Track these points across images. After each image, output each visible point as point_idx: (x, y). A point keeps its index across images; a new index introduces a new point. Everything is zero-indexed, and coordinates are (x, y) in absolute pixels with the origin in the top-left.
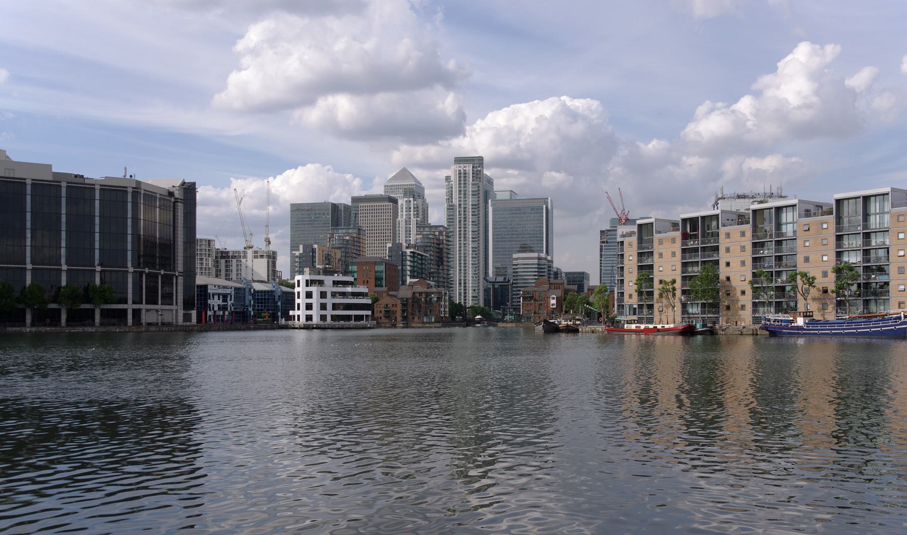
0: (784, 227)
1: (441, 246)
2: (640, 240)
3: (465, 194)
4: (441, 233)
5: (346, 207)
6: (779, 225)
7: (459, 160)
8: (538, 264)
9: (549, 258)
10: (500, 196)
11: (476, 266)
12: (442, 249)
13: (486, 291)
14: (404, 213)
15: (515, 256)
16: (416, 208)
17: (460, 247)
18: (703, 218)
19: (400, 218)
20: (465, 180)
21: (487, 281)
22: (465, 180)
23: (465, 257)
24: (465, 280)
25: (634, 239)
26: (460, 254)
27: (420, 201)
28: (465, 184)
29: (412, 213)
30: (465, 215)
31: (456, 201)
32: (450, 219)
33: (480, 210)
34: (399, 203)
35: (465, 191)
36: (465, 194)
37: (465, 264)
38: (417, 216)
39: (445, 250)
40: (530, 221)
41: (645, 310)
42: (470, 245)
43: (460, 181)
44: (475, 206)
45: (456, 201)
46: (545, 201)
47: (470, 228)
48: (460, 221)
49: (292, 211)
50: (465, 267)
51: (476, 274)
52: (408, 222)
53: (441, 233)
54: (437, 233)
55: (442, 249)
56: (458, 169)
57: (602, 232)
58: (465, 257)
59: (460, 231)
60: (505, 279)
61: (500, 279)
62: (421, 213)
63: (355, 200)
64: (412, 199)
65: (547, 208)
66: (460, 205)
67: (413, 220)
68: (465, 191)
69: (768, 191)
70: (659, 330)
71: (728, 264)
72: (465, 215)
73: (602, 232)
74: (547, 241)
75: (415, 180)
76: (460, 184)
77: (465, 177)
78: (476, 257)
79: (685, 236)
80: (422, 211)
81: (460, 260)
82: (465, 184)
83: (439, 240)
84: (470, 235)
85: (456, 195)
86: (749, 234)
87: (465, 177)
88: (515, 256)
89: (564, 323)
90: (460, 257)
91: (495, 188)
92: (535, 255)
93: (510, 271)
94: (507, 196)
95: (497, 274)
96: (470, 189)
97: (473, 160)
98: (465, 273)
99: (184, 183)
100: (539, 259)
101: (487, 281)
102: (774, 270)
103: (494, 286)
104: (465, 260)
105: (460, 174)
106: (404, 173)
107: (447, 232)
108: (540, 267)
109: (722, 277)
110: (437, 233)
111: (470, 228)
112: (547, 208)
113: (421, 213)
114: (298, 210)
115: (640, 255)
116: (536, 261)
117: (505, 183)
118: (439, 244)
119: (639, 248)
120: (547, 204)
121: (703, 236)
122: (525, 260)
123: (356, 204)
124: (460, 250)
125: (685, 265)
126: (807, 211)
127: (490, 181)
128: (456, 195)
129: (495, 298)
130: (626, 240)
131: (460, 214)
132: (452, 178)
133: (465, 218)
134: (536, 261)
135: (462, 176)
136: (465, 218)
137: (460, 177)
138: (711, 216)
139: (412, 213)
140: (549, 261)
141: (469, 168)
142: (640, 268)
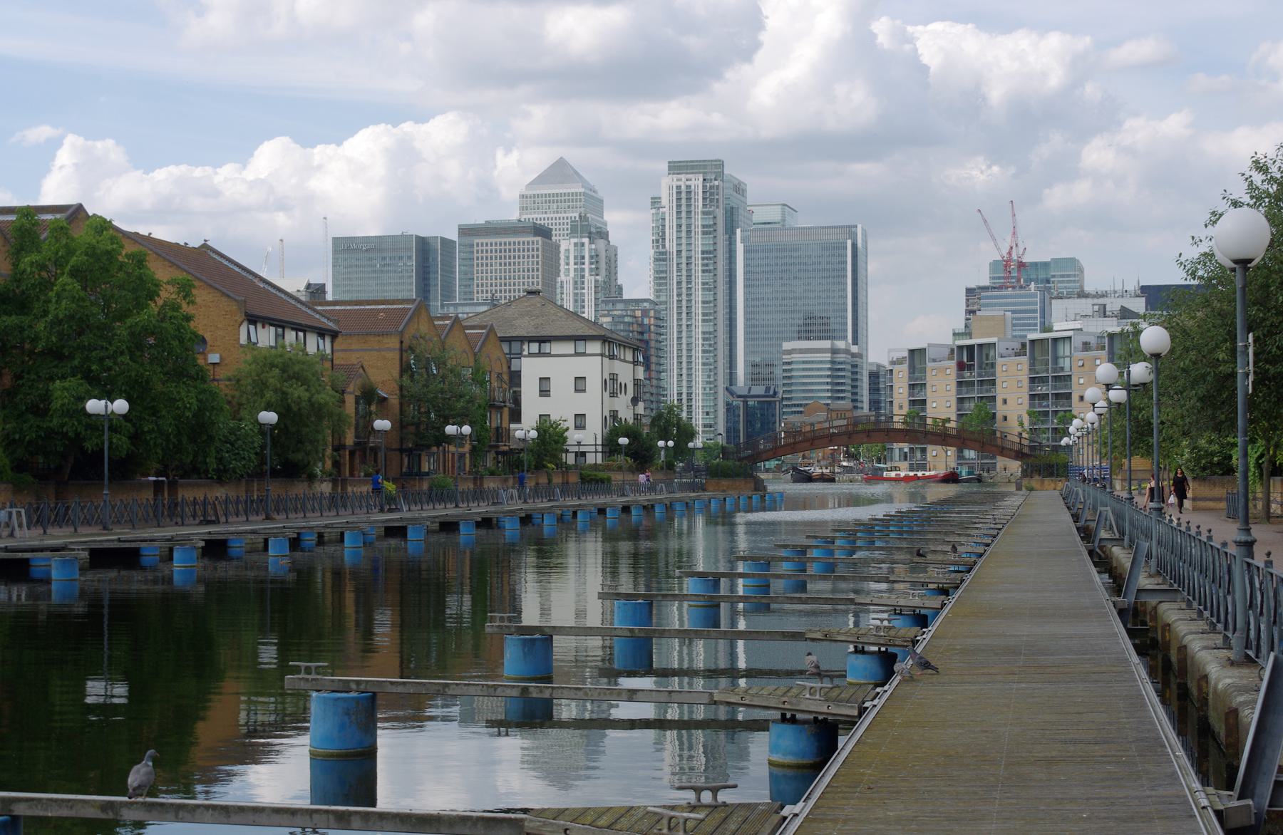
0: (1061, 361)
1: (646, 337)
2: (912, 369)
3: (689, 232)
4: (645, 313)
5: (446, 243)
6: (1056, 358)
7: (676, 168)
8: (833, 362)
9: (854, 349)
10: (760, 215)
11: (710, 367)
12: (647, 342)
13: (730, 408)
14: (572, 267)
15: (787, 346)
16: (595, 258)
17: (680, 332)
18: (981, 346)
19: (562, 277)
20: (689, 206)
21: (732, 393)
22: (689, 206)
23: (689, 350)
24: (689, 394)
25: (905, 367)
26: (680, 344)
27: (601, 244)
28: (689, 212)
29: (586, 267)
30: (689, 270)
31: (671, 246)
32: (661, 278)
33: (719, 264)
34: (562, 249)
35: (689, 226)
36: (689, 232)
37: (689, 363)
38: (596, 272)
39: (653, 344)
40: (822, 272)
41: (918, 454)
42: (699, 328)
43: (679, 206)
44: (709, 254)
45: (671, 246)
46: (850, 230)
47: (699, 296)
48: (679, 283)
49: (335, 252)
50: (689, 369)
51: (711, 383)
52: (579, 282)
53: (645, 313)
54: (638, 313)
55: (647, 342)
56: (675, 183)
57: (970, 292)
58: (689, 350)
59: (679, 301)
60: (768, 389)
61: (759, 390)
62: (603, 265)
63: (466, 231)
64: (586, 240)
65: (854, 246)
66: (679, 252)
67: (589, 280)
68: (689, 226)
69: (1119, 287)
70: (919, 478)
71: (1005, 402)
72: (689, 270)
73: (970, 292)
74: (855, 311)
75: (585, 184)
76: (679, 213)
77: (689, 199)
78: (710, 350)
79: (961, 367)
80: (607, 264)
81: (679, 357)
82: (689, 212)
83: (641, 325)
84: (698, 309)
85: (671, 233)
86: (1026, 367)
87: (689, 199)
88: (787, 346)
89: (818, 471)
90: (680, 350)
91: (750, 199)
92: (826, 344)
93: (778, 372)
94: (774, 214)
95: (754, 379)
96: (698, 221)
97: (705, 167)
98: (689, 381)
99: (309, 286)
100: (834, 351)
101: (732, 393)
102: (1050, 409)
103: (745, 403)
104: (689, 357)
105: (679, 193)
106: (560, 171)
107: (655, 309)
108: (835, 368)
109: (999, 416)
110: (638, 313)
111: (699, 296)
112: (854, 246)
113: (603, 265)
114: (348, 250)
115: (912, 387)
116: (828, 356)
117: (765, 194)
118: (642, 333)
119: (910, 379)
120: (853, 236)
121: (980, 367)
122: (807, 356)
123: (467, 240)
124: (679, 338)
125: (960, 401)
126: (1085, 344)
127: (739, 189)
128: (671, 233)
129: (749, 422)
130: (896, 368)
131: (679, 270)
132: (665, 202)
133: (689, 276)
134: (828, 356)
135: (683, 197)
136: (689, 276)
137: (679, 199)
138: (989, 344)
139: (586, 267)
140: (854, 355)
141: (697, 182)
142: (913, 403)
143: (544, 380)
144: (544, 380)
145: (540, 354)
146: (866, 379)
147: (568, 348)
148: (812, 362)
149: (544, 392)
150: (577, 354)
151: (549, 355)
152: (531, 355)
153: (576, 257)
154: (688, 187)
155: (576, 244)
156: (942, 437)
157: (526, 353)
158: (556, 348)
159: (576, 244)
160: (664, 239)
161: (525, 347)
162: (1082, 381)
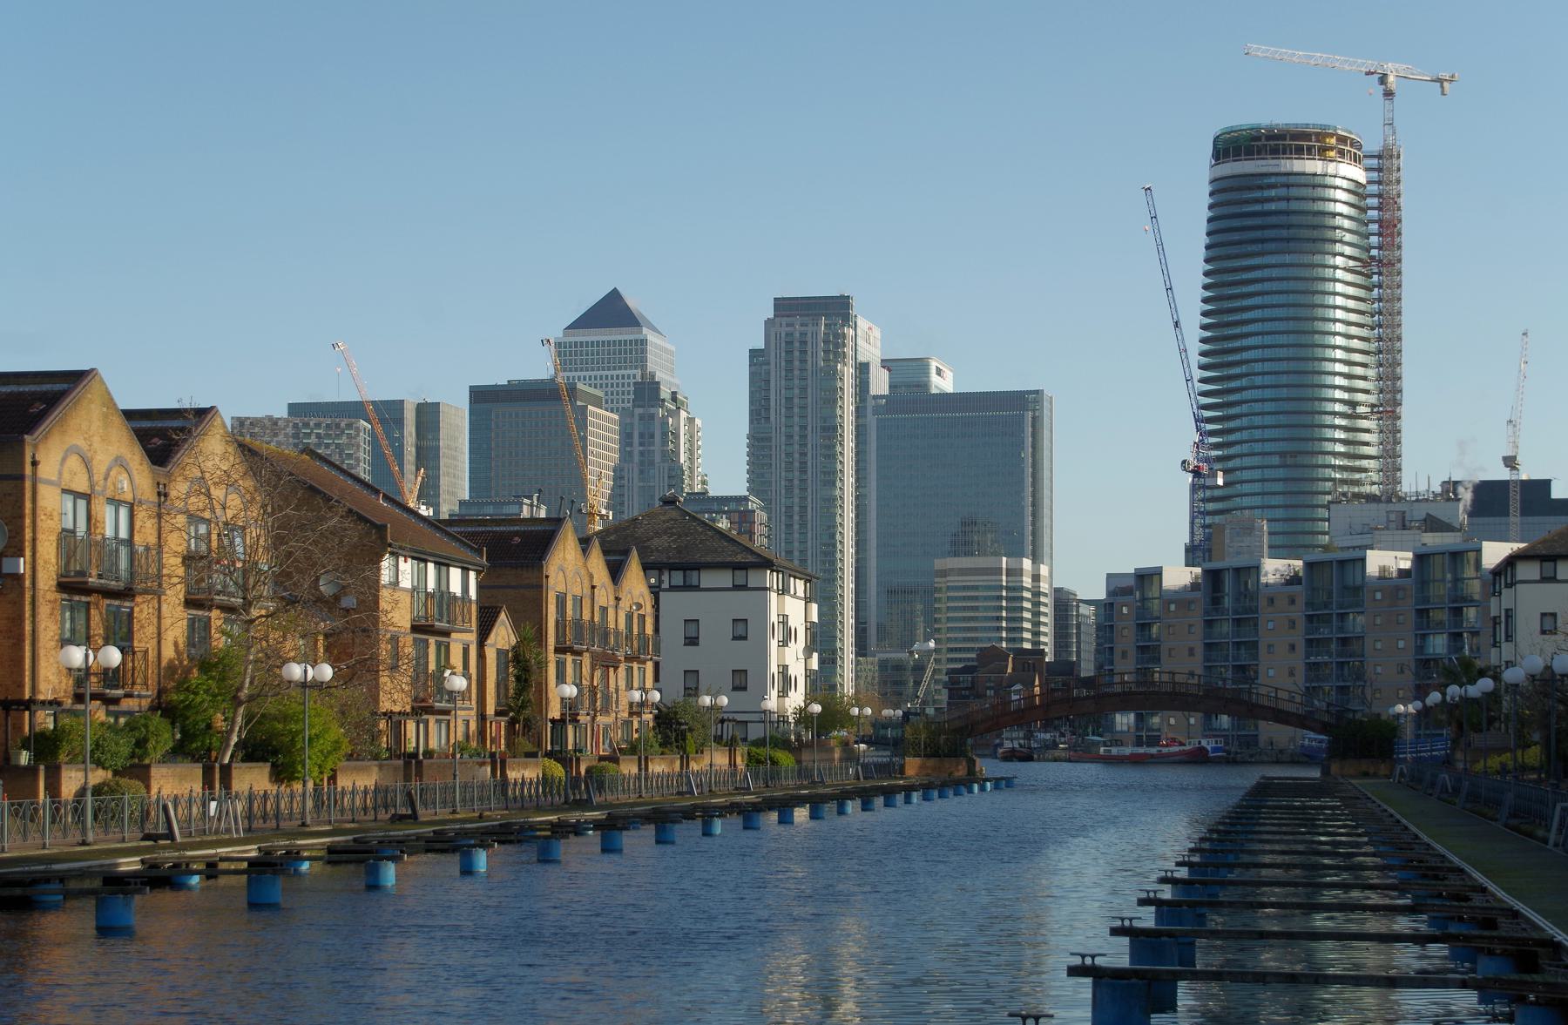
137: (789, 352)
143: (1270, 646)
144: (1270, 646)
145: (687, 587)
146: (1047, 609)
147: (725, 578)
148: (976, 588)
149: (692, 641)
150: (736, 588)
151: (697, 588)
152: (672, 588)
153: (641, 435)
154: (803, 334)
155: (642, 418)
156: (1176, 699)
157: (666, 585)
158: (708, 579)
159: (642, 418)
160: (768, 410)
161: (665, 577)
162: (1379, 645)
